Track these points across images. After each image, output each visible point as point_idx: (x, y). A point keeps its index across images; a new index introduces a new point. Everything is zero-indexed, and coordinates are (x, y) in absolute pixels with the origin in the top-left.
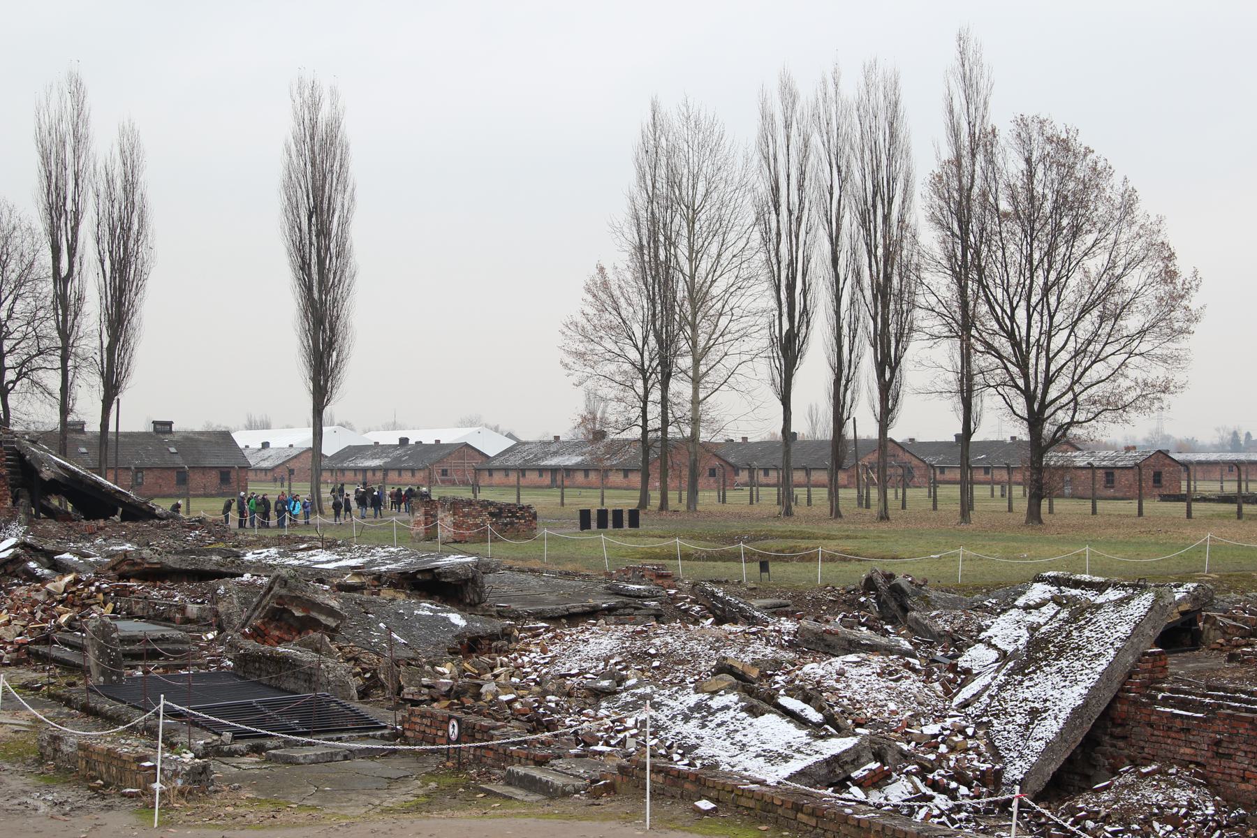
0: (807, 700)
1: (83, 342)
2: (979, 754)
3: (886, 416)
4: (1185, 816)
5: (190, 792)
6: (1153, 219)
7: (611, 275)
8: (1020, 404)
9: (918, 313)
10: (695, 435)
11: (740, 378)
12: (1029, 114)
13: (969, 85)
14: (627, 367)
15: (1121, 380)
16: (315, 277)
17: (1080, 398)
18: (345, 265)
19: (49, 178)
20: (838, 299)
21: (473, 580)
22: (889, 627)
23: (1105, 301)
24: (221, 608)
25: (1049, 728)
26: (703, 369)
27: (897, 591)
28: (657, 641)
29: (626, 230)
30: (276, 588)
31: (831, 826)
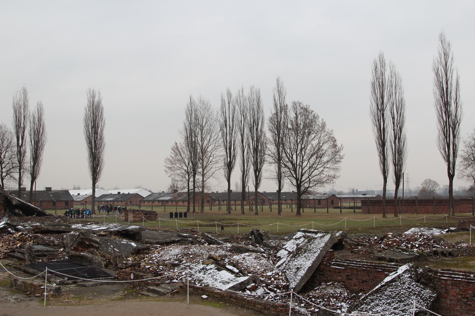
0: (234, 266)
1: (26, 164)
2: (283, 281)
5: (55, 295)
6: (330, 130)
8: (294, 182)
9: (266, 156)
12: (296, 101)
14: (183, 171)
16: (93, 146)
17: (311, 180)
19: (16, 117)
20: (243, 152)
21: (138, 233)
22: (258, 245)
24: (65, 241)
25: (302, 273)
26: (205, 172)
27: (260, 235)
28: (191, 250)
30: (81, 236)
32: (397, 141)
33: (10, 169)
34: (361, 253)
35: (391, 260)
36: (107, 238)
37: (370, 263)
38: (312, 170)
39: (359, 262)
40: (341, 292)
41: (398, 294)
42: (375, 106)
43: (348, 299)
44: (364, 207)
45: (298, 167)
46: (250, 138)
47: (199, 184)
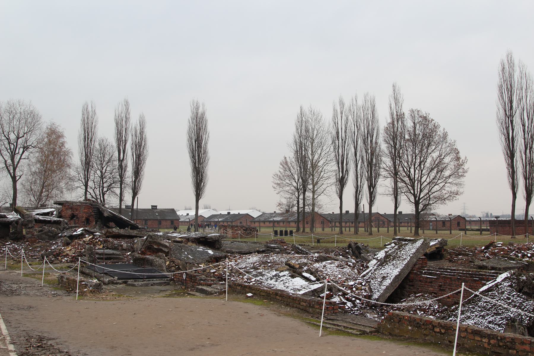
0: (311, 274)
1: (127, 179)
2: (365, 291)
3: (371, 203)
4: (428, 309)
5: (94, 291)
6: (453, 141)
7: (288, 160)
8: (412, 199)
9: (382, 170)
10: (313, 209)
11: (327, 191)
12: (414, 109)
13: (396, 100)
14: (293, 188)
15: (443, 191)
16: (197, 160)
17: (431, 196)
19: (118, 130)
20: (357, 166)
21: (218, 241)
22: (349, 256)
23: (439, 166)
24: (135, 246)
25: (388, 282)
26: (316, 189)
27: (358, 248)
28: (271, 258)
29: (292, 146)
30: (149, 239)
31: (286, 300)
32: (528, 151)
33: (111, 184)
34: (460, 262)
35: (493, 268)
36: (181, 245)
37: (467, 271)
38: (433, 186)
39: (454, 270)
40: (430, 305)
41: (494, 305)
42: (502, 112)
43: (438, 312)
44: (492, 228)
45: (416, 182)
46: (364, 151)
47: (309, 201)
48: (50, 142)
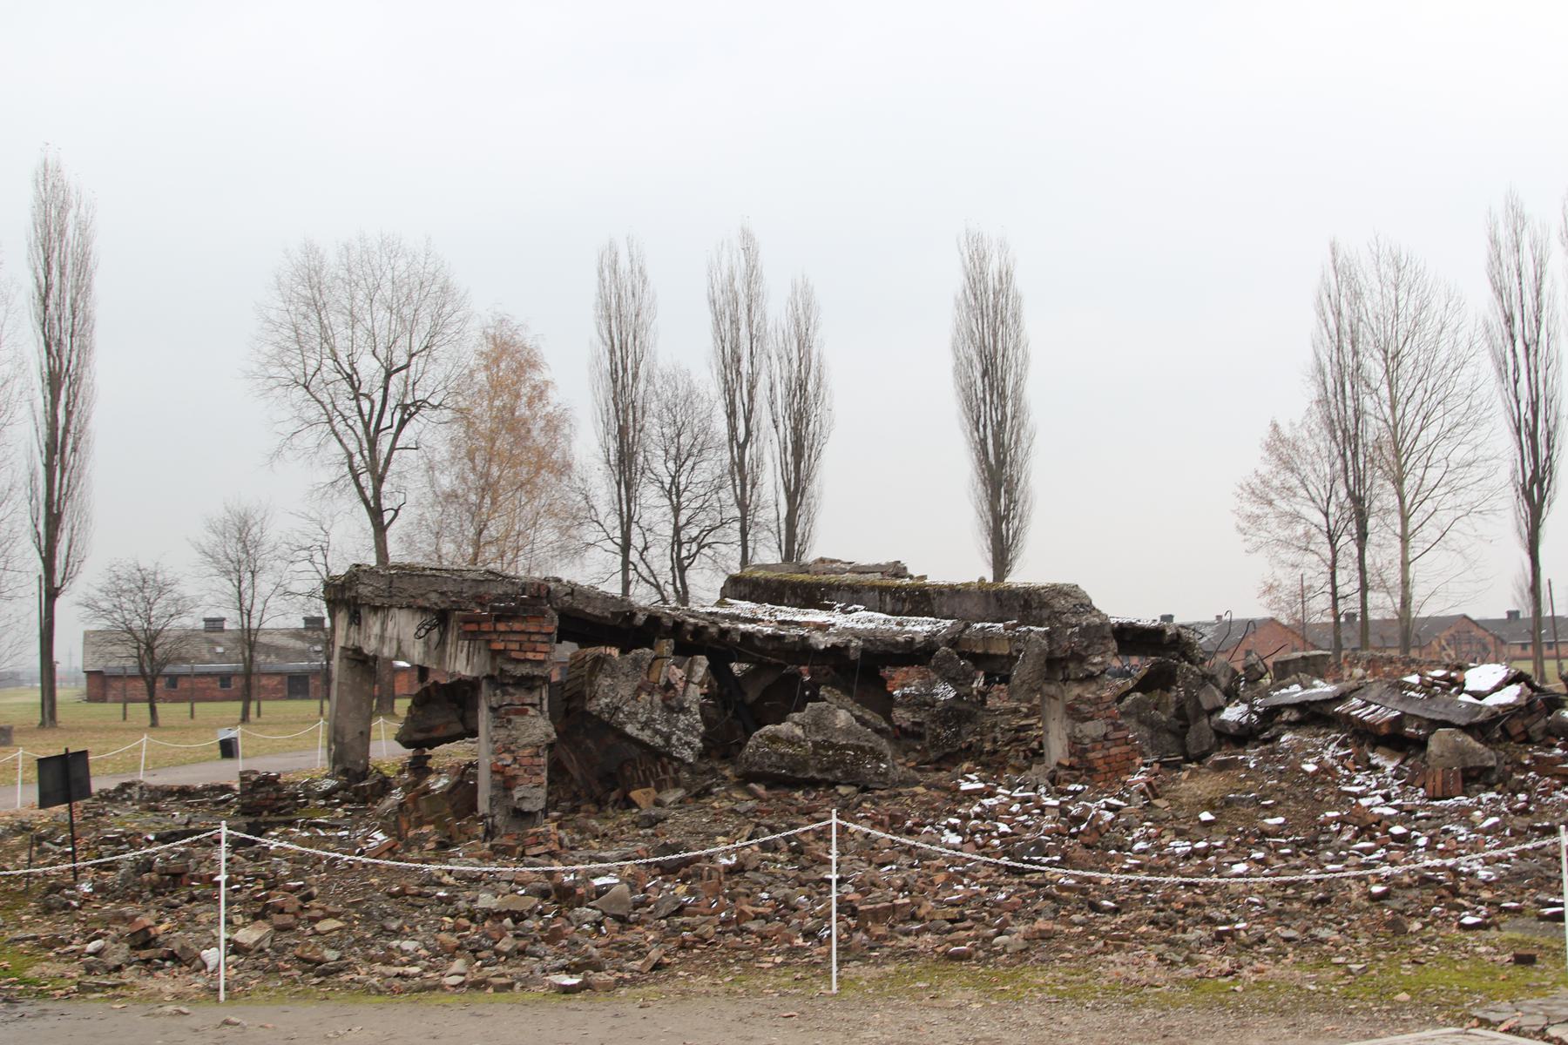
18: (1021, 425)
48: (497, 386)
